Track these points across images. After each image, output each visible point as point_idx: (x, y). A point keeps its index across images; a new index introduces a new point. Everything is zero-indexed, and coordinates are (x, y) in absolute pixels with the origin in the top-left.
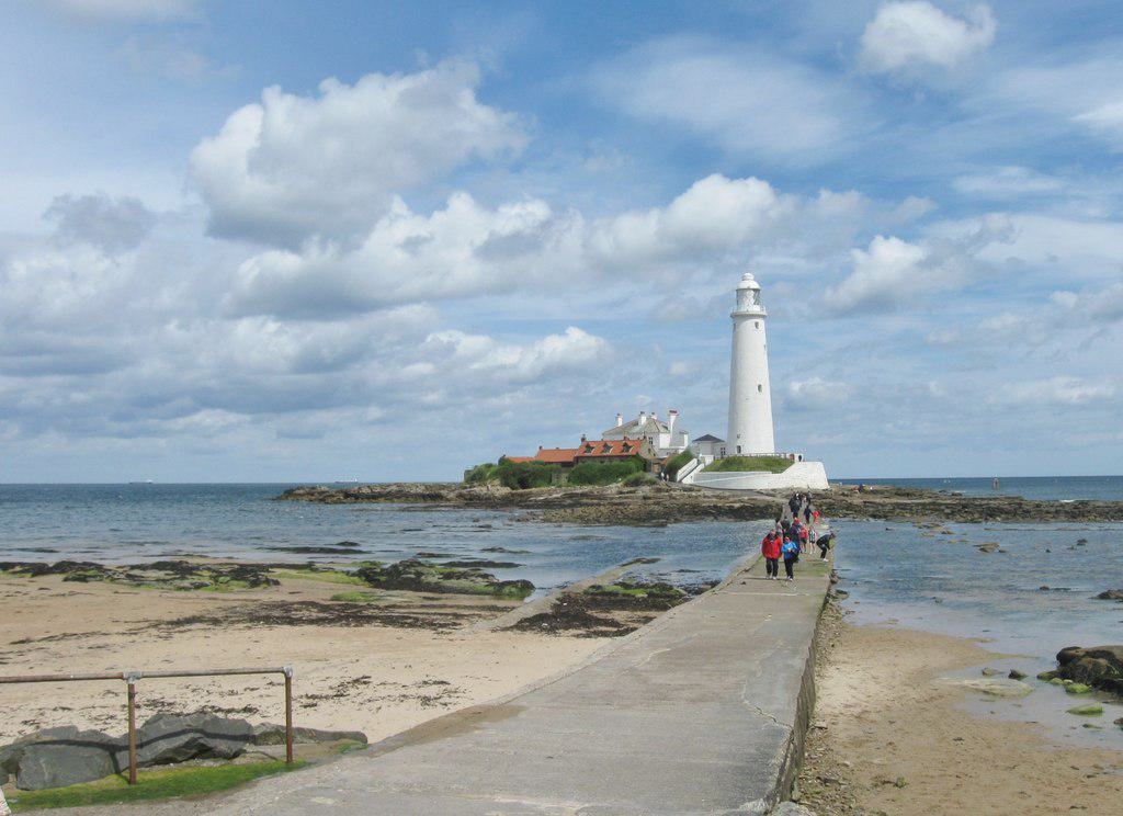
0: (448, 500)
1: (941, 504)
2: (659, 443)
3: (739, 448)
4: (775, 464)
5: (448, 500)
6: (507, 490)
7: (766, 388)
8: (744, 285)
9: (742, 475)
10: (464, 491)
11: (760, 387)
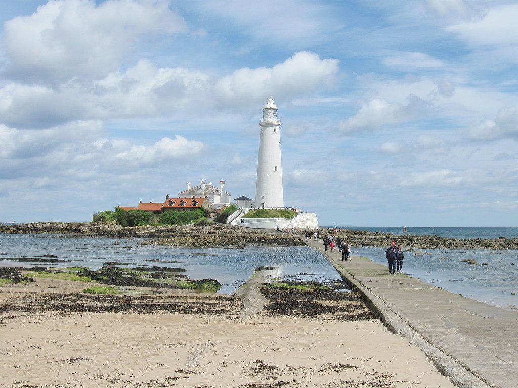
0: (84, 233)
4: (289, 214)
5: (84, 233)
8: (268, 106)
9: (266, 220)
10: (94, 228)
11: (276, 168)
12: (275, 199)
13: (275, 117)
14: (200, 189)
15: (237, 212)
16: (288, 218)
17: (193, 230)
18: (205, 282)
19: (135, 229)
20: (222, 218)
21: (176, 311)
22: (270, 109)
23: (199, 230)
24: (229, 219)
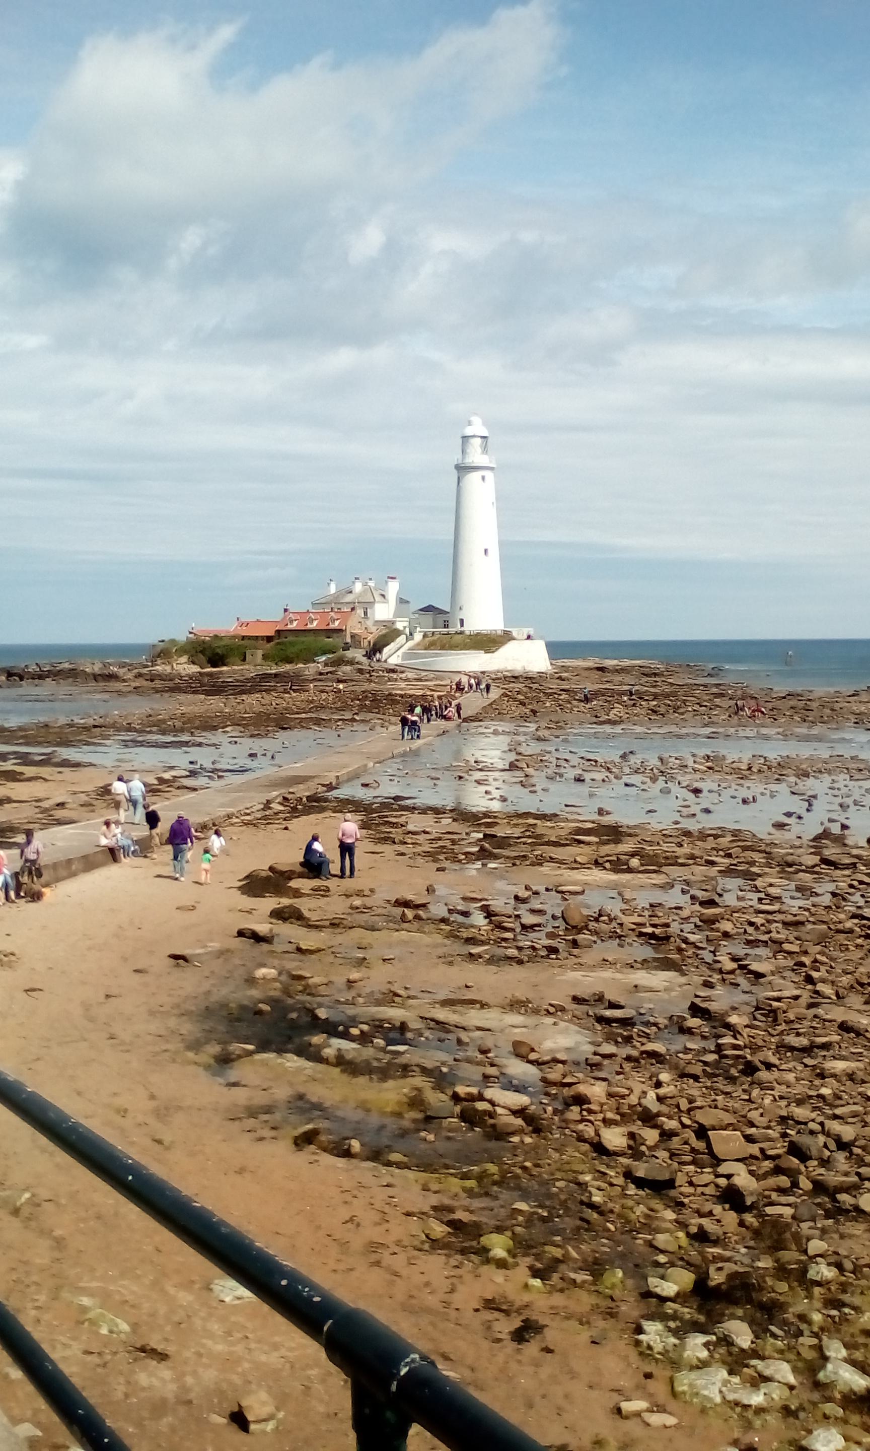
0: (124, 681)
1: (396, 695)
2: (373, 614)
3: (462, 621)
4: (488, 642)
5: (124, 681)
6: (195, 669)
7: (494, 552)
8: (469, 431)
9: (451, 655)
10: (145, 671)
11: (486, 551)
14: (351, 592)
15: (402, 639)
17: (321, 674)
18: (27, 836)
19: (221, 672)
21: (322, 810)
22: (474, 436)
23: (330, 672)
24: (386, 650)
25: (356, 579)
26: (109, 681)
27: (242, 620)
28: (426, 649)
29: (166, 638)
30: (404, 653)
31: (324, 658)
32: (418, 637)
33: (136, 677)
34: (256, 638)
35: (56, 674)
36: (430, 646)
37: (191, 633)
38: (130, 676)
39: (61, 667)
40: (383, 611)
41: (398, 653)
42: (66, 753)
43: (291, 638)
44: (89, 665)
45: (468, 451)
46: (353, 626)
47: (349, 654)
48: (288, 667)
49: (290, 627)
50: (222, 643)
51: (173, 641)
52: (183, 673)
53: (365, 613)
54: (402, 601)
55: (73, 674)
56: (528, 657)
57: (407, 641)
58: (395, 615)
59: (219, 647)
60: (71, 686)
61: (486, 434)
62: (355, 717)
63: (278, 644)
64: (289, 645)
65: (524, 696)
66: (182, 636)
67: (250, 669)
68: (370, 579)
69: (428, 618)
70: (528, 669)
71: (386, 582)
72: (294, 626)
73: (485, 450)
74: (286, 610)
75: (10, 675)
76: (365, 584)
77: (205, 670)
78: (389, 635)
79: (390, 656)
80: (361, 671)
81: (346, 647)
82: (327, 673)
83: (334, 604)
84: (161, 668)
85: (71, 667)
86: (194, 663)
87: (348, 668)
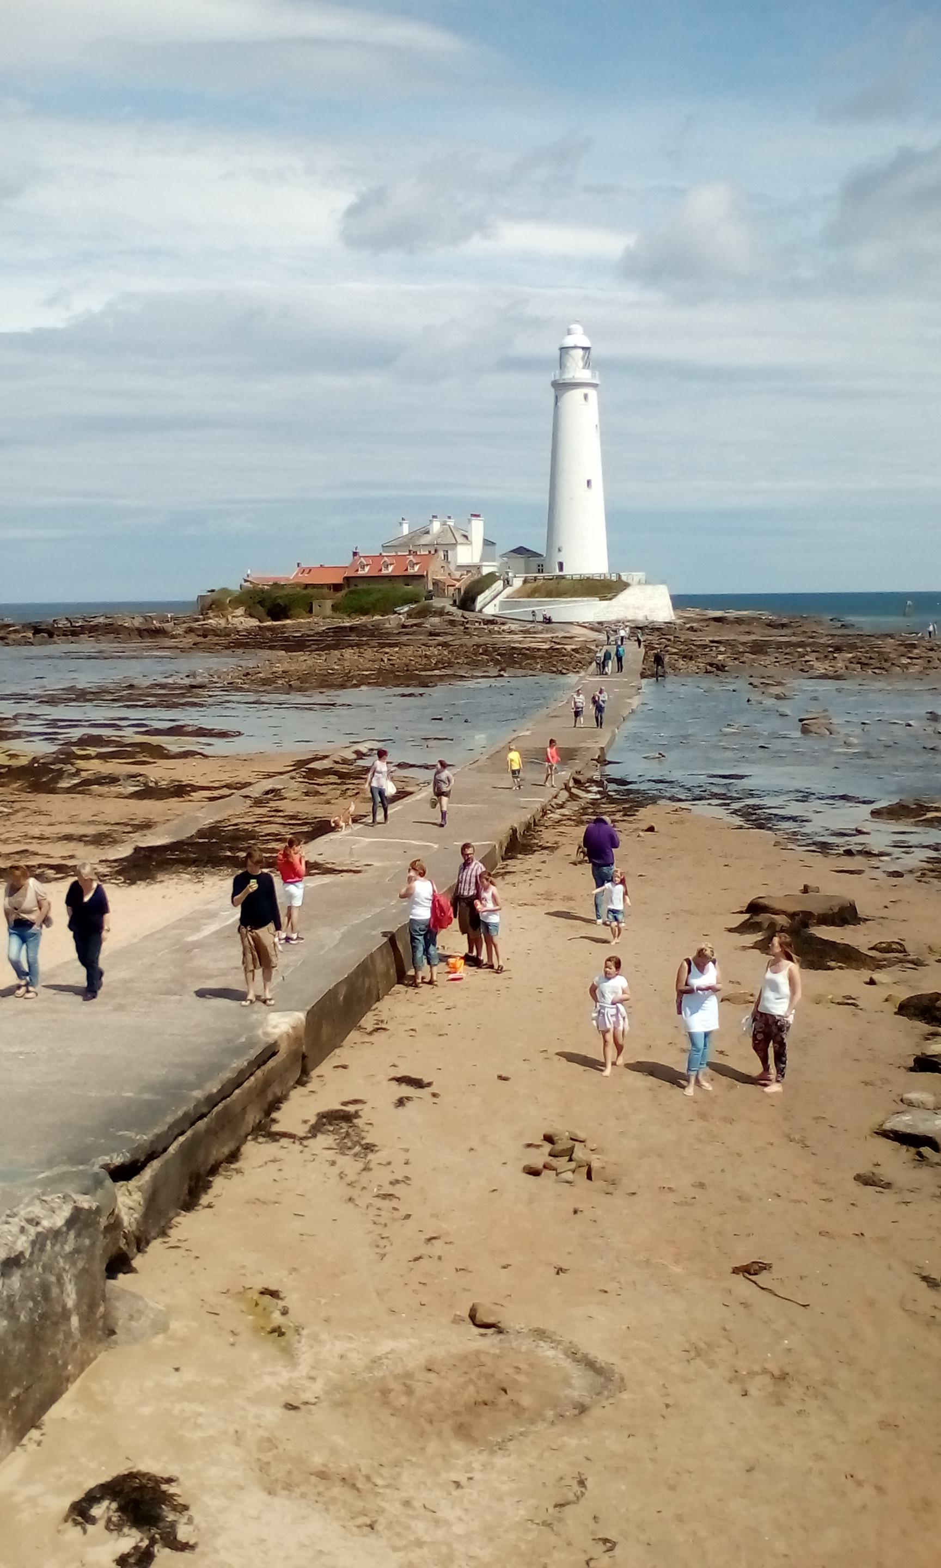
3: (561, 566)
4: (604, 588)
5: (173, 637)
6: (254, 622)
7: (598, 483)
8: (569, 341)
10: (195, 625)
11: (589, 482)
12: (586, 555)
13: (587, 365)
14: (428, 533)
15: (499, 584)
16: (603, 598)
17: (404, 626)
20: (467, 601)
22: (575, 347)
23: (415, 625)
24: (481, 600)
25: (434, 517)
26: (156, 637)
27: (303, 565)
28: (529, 597)
29: (216, 588)
30: (502, 602)
31: (406, 609)
32: (517, 583)
33: (186, 632)
34: (322, 586)
35: (94, 630)
36: (531, 595)
37: (246, 581)
38: (180, 630)
39: (96, 621)
40: (467, 555)
41: (494, 602)
42: (189, 717)
43: (362, 586)
44: (128, 619)
45: (568, 364)
46: (435, 572)
47: (437, 603)
48: (364, 619)
49: (361, 573)
50: (284, 592)
51: (225, 591)
52: (240, 627)
53: (446, 556)
54: (487, 543)
55: (111, 630)
56: (649, 603)
57: (504, 588)
58: (482, 560)
59: (281, 597)
60: (113, 642)
61: (587, 344)
62: (502, 673)
63: (351, 592)
64: (362, 594)
65: (662, 651)
66: (234, 584)
67: (322, 619)
68: (449, 517)
69: (520, 561)
70: (651, 619)
71: (470, 521)
72: (366, 571)
73: (587, 365)
74: (355, 554)
75: (37, 630)
76: (444, 524)
77: (265, 624)
78: (481, 584)
79: (485, 605)
80: (452, 623)
81: (429, 597)
82: (412, 626)
83: (409, 545)
84: (214, 622)
85: (107, 621)
86: (251, 616)
87: (436, 620)
